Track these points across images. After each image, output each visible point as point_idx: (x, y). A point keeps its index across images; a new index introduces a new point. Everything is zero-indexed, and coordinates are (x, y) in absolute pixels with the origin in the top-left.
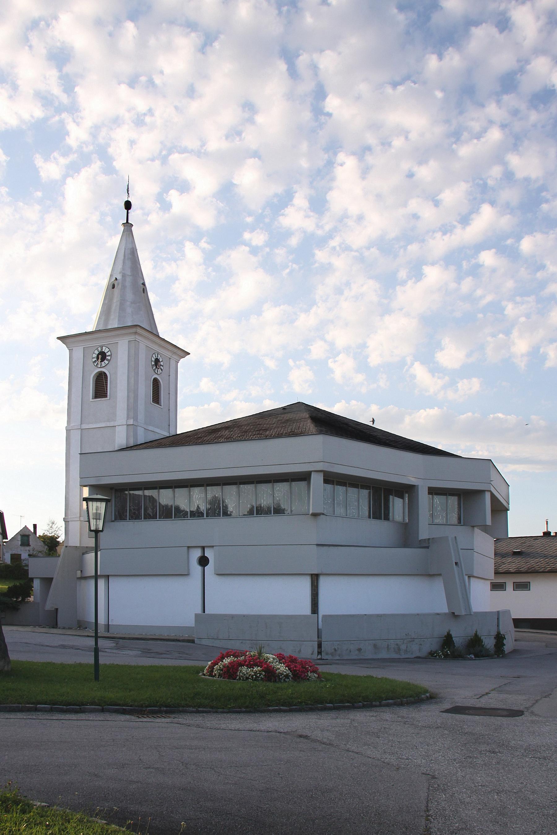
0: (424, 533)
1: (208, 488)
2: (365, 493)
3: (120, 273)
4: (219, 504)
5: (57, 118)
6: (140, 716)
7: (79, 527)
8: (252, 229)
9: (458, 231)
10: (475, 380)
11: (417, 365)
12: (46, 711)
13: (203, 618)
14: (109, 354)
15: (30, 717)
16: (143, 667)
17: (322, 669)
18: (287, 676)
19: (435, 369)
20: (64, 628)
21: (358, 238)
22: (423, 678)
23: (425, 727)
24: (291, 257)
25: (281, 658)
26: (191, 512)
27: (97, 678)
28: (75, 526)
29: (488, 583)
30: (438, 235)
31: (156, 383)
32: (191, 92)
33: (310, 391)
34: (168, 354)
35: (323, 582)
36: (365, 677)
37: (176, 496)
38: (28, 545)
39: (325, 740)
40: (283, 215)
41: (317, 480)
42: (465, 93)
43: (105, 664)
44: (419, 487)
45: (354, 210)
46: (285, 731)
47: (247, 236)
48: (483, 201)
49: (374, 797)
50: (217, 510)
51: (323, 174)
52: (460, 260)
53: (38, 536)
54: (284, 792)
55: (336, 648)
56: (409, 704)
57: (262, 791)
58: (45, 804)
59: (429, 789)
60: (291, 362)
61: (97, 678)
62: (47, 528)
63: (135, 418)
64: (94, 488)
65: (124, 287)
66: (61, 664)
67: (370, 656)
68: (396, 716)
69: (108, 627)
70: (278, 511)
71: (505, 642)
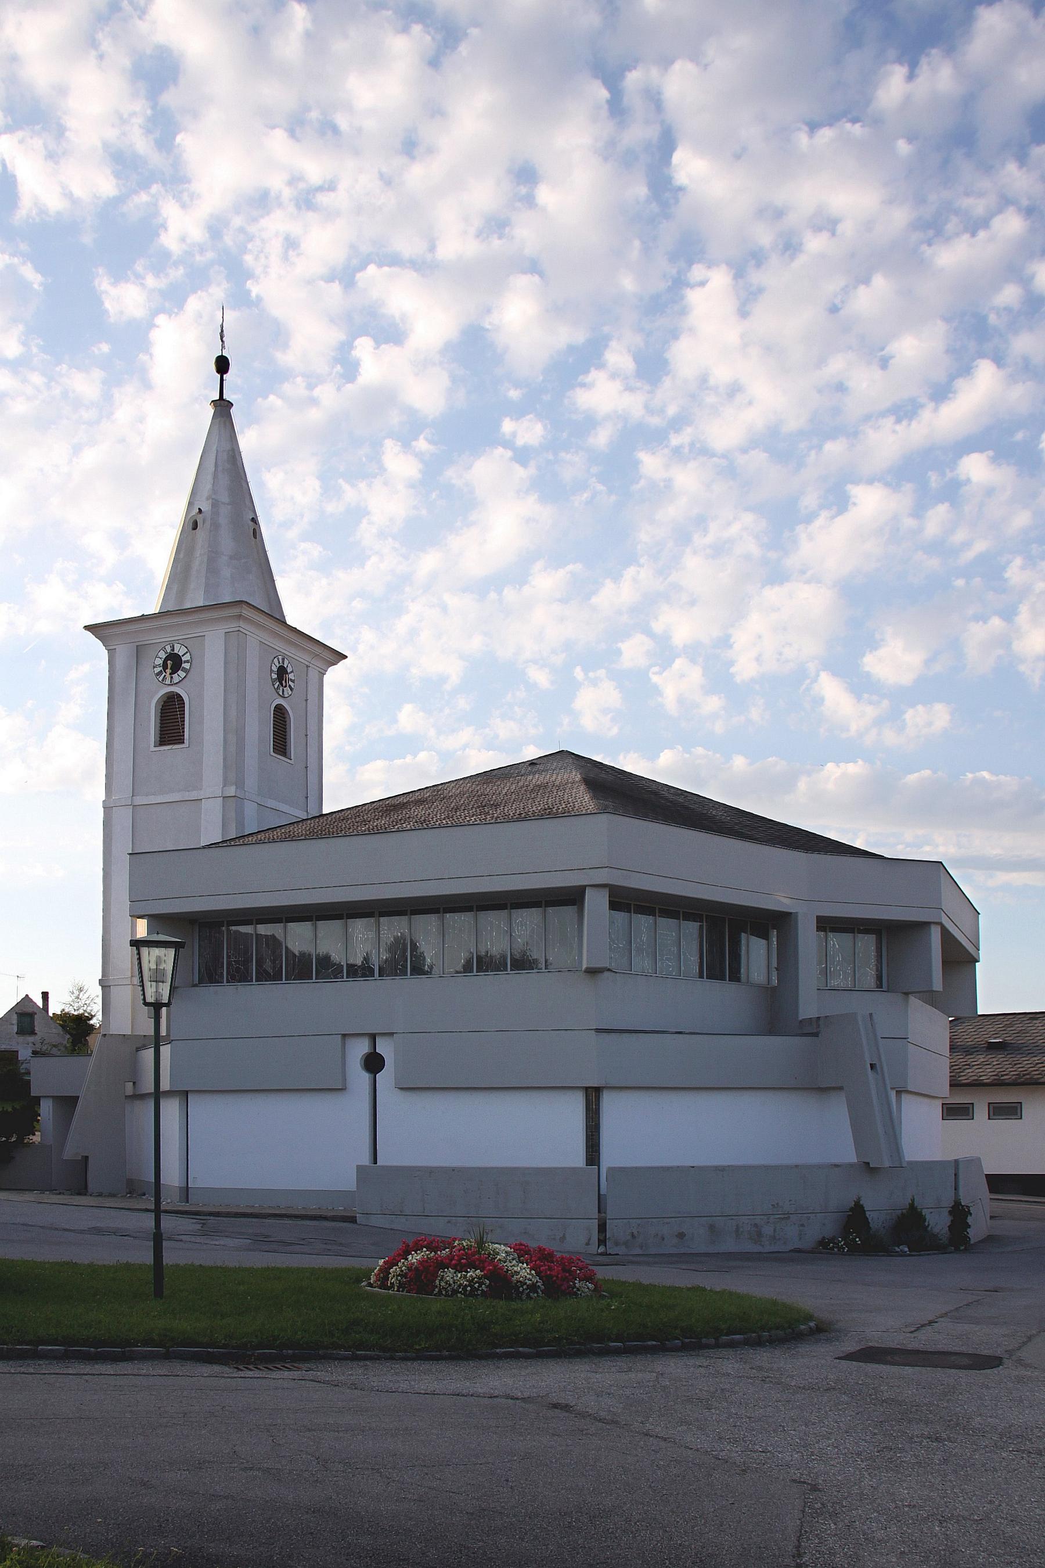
0: (808, 1007)
1: (382, 919)
2: (692, 928)
3: (207, 499)
4: (405, 950)
5: (144, 198)
6: (241, 1367)
7: (130, 997)
8: (518, 411)
9: (926, 415)
10: (939, 707)
11: (825, 678)
12: (55, 1358)
13: (372, 1173)
14: (187, 657)
15: (22, 1370)
16: (251, 1271)
17: (602, 1273)
18: (533, 1287)
19: (862, 686)
20: (100, 1195)
21: (725, 431)
22: (804, 1291)
23: (804, 1388)
24: (594, 470)
25: (522, 1252)
26: (350, 967)
27: (159, 1293)
28: (125, 995)
29: (938, 1104)
30: (889, 422)
31: (280, 715)
32: (410, 147)
33: (615, 730)
34: (303, 657)
35: (609, 1103)
36: (689, 1289)
37: (319, 935)
38: (33, 1033)
39: (603, 1414)
40: (583, 385)
41: (596, 903)
42: (957, 142)
43: (177, 1265)
44: (800, 918)
45: (722, 374)
46: (526, 1395)
47: (508, 426)
48: (982, 355)
49: (693, 1527)
50: (405, 962)
51: (664, 307)
52: (927, 474)
53: (51, 1015)
54: (514, 1516)
55: (636, 1233)
56: (774, 1342)
57: (472, 1514)
58: (34, 1543)
59: (803, 1512)
60: (578, 673)
61: (159, 1293)
62: (69, 999)
63: (240, 784)
64: (157, 920)
65: (215, 526)
66: (91, 1265)
67: (703, 1249)
68: (747, 1367)
69: (186, 1191)
70: (522, 963)
71: (970, 1220)
